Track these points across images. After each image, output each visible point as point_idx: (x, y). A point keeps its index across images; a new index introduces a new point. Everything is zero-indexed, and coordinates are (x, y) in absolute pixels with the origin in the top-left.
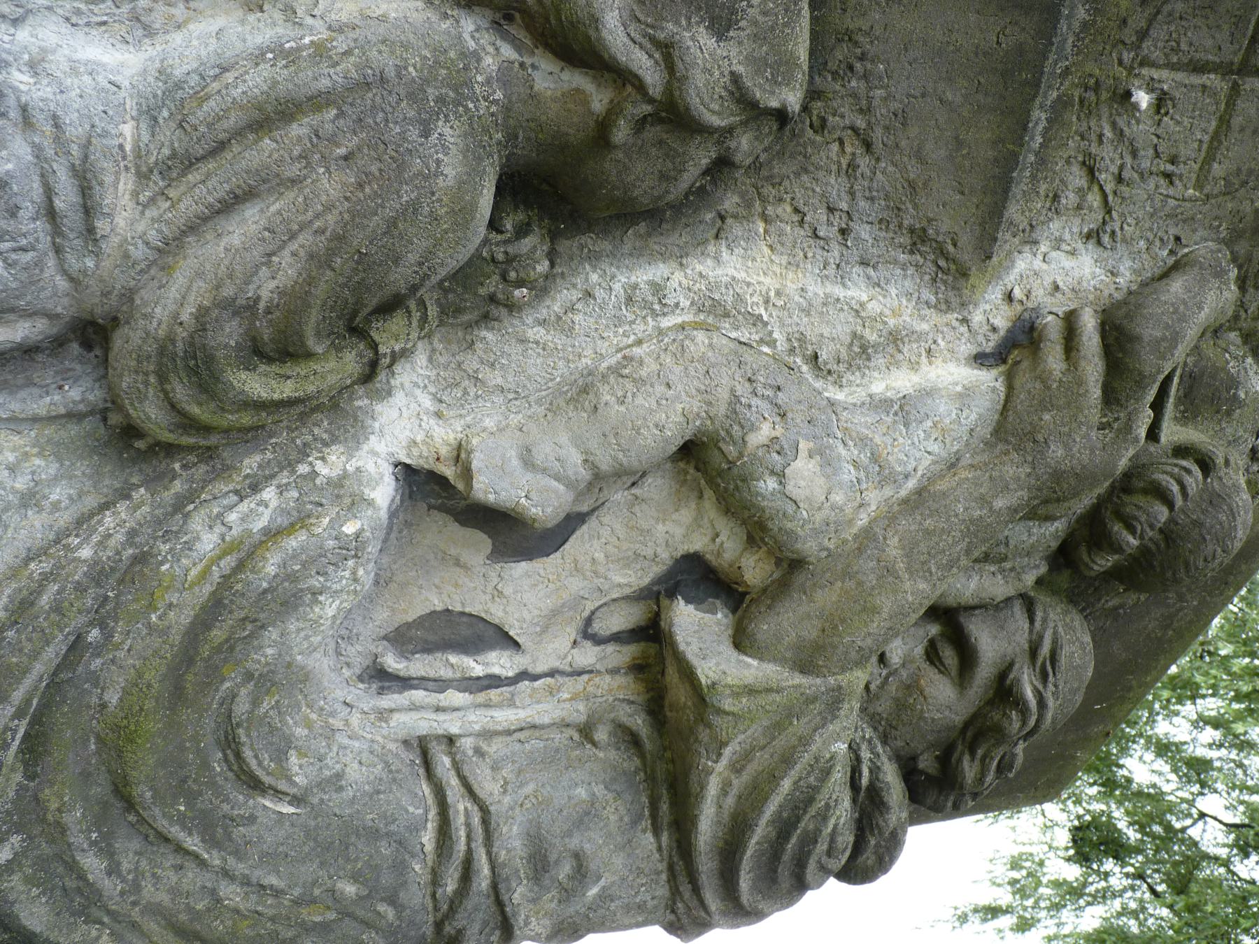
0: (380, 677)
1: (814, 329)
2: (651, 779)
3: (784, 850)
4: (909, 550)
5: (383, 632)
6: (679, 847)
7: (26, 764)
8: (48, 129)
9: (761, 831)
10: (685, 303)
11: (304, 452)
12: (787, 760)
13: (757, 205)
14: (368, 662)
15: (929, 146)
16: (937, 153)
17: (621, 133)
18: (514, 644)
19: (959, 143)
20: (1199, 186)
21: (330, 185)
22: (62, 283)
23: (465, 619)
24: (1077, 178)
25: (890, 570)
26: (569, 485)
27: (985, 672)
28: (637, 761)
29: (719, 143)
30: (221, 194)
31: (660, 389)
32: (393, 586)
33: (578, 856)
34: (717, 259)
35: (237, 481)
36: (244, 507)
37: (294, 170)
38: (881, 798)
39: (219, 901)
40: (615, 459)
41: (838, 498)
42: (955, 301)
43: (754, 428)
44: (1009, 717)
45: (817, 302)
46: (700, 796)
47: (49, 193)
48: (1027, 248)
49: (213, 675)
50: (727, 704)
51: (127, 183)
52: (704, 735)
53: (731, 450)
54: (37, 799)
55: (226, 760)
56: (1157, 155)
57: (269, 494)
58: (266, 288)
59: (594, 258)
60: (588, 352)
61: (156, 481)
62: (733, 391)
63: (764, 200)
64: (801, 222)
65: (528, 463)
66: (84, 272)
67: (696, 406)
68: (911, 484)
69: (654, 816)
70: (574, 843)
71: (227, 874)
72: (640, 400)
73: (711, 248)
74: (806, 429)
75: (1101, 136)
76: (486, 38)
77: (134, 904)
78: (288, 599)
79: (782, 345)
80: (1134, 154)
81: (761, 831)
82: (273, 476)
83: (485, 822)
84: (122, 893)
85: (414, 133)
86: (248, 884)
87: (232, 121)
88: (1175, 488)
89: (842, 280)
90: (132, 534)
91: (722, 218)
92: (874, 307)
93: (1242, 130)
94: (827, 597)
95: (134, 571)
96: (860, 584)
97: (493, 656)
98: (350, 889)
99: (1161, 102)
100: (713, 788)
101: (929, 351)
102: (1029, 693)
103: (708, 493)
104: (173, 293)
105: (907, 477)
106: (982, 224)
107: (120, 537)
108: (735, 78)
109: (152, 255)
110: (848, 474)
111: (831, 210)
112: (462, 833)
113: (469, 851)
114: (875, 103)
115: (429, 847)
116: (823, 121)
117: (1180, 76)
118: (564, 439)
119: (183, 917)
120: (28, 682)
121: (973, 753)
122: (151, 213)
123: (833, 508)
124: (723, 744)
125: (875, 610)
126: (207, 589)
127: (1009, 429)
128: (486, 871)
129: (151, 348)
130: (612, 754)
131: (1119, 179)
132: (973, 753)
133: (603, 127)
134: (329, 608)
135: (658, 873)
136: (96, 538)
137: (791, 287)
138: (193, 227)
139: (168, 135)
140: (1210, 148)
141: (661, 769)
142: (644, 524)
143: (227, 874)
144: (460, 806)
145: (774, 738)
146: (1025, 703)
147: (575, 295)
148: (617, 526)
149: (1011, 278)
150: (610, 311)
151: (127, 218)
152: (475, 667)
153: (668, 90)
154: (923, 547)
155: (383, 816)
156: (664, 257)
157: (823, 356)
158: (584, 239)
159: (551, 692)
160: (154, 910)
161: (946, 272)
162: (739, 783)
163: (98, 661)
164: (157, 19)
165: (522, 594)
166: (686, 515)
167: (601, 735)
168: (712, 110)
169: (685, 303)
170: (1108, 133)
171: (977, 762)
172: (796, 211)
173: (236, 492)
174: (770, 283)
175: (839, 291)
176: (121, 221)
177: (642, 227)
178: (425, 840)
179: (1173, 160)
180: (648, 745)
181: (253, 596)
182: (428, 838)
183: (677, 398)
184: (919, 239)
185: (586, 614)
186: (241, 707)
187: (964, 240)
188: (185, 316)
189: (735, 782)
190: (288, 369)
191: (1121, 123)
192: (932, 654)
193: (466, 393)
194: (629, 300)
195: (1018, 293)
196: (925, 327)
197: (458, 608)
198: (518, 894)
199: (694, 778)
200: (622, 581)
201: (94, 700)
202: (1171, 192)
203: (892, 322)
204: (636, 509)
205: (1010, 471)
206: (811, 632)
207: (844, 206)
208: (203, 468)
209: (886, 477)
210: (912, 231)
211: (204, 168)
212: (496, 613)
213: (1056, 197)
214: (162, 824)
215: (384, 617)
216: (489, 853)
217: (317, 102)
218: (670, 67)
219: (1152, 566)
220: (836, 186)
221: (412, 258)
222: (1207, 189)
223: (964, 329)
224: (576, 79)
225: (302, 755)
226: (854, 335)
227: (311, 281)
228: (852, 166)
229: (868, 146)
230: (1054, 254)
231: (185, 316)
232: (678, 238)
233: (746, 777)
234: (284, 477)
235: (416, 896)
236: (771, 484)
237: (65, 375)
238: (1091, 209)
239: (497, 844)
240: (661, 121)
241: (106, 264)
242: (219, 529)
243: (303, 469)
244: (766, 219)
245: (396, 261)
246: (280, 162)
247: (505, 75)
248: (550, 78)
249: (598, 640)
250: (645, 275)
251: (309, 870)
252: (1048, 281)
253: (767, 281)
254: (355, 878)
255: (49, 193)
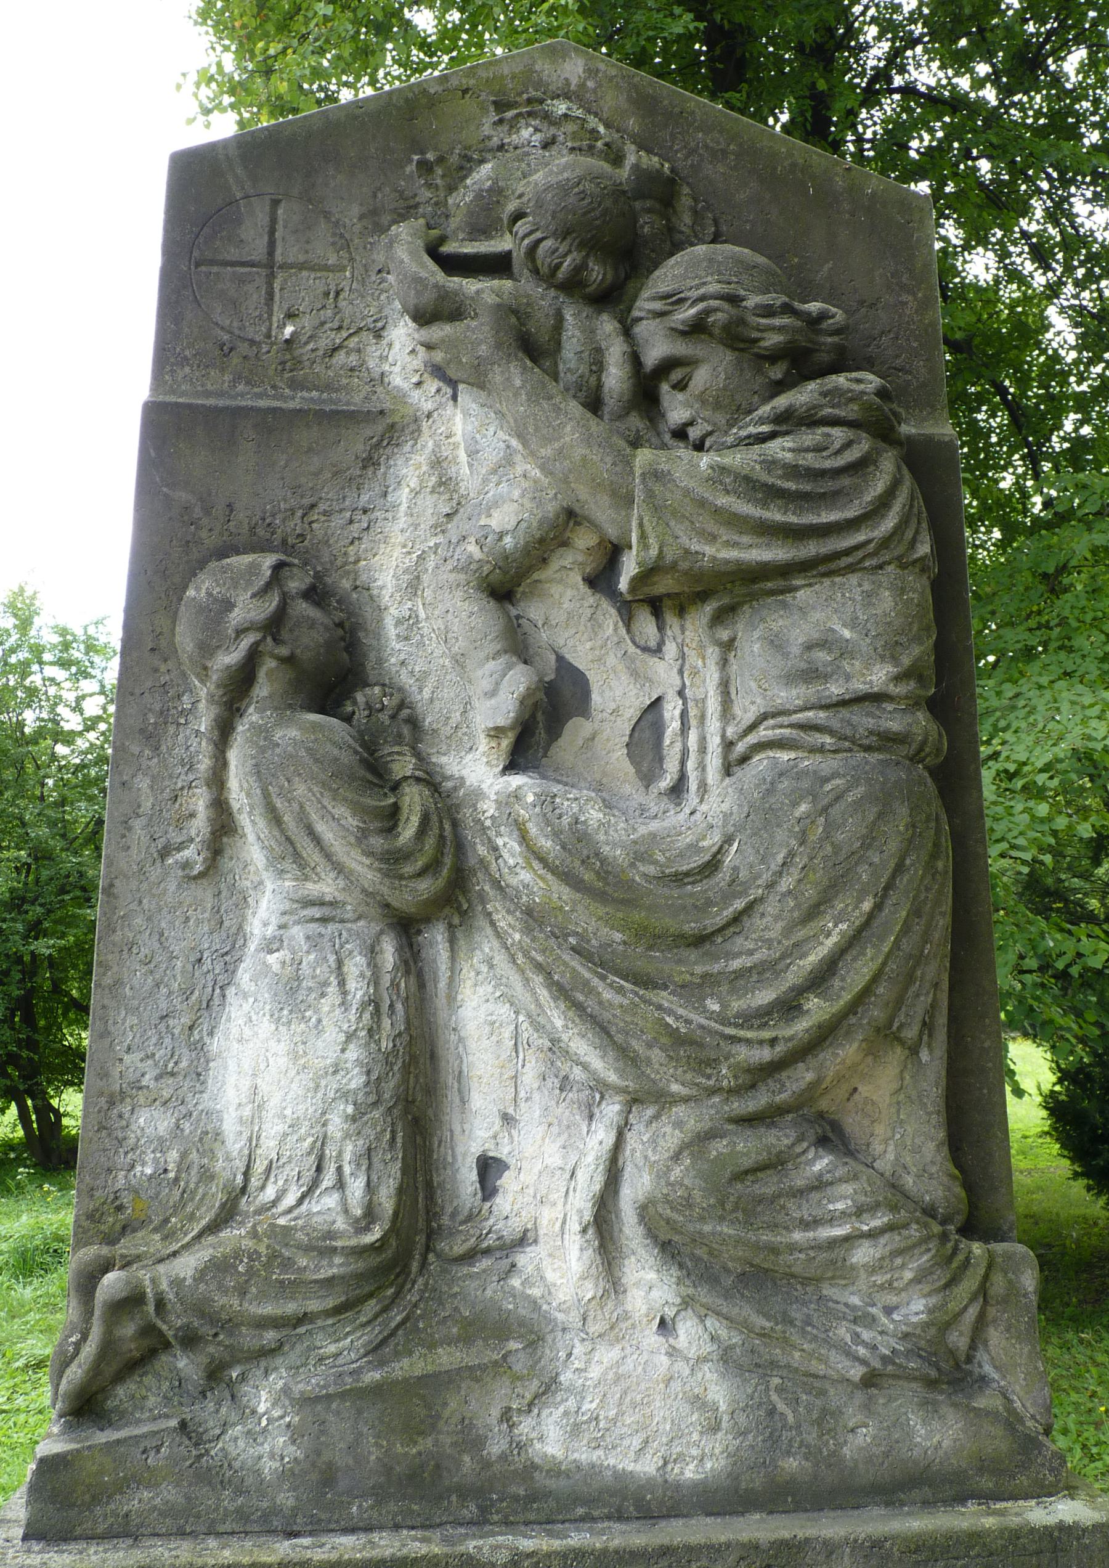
0: (678, 790)
1: (428, 519)
2: (753, 597)
3: (797, 491)
4: (547, 440)
5: (642, 789)
6: (805, 571)
7: (655, 988)
8: (287, 917)
9: (775, 515)
10: (409, 604)
11: (478, 821)
12: (702, 503)
13: (350, 567)
14: (665, 798)
15: (312, 469)
16: (316, 462)
17: (284, 651)
18: (657, 703)
19: (310, 450)
20: (343, 269)
21: (300, 789)
22: (361, 923)
23: (636, 735)
24: (340, 358)
25: (560, 451)
26: (510, 667)
27: (681, 348)
28: (746, 607)
29: (293, 598)
30: (309, 840)
31: (450, 616)
32: (604, 781)
33: (809, 647)
34: (381, 588)
35: (491, 858)
36: (506, 855)
37: (295, 806)
38: (782, 413)
39: (790, 892)
40: (492, 641)
41: (516, 494)
42: (413, 427)
43: (470, 556)
44: (714, 322)
45: (410, 520)
46: (738, 562)
47: (313, 920)
48: (386, 380)
49: (630, 885)
50: (654, 552)
51: (310, 885)
52: (684, 565)
53: (486, 569)
54: (682, 987)
55: (693, 883)
56: (324, 307)
57: (500, 842)
58: (352, 822)
59: (380, 662)
60: (441, 661)
61: (483, 898)
62: (451, 571)
63: (346, 564)
64: (359, 539)
65: (492, 693)
66: (355, 911)
67: (459, 594)
68: (514, 443)
69: (782, 592)
70: (795, 650)
71: (771, 886)
72: (455, 629)
73: (375, 592)
74: (473, 521)
75: (313, 350)
76: (245, 720)
77: (779, 942)
78: (577, 839)
79: (440, 539)
80: (323, 324)
81: (775, 515)
82: (489, 839)
83: (774, 715)
84: (769, 949)
85: (278, 751)
86: (781, 873)
87: (276, 833)
88: (526, 242)
89: (396, 506)
90: (509, 912)
91: (356, 587)
92: (414, 483)
93: (307, 252)
94: (583, 492)
95: (533, 917)
96: (570, 471)
97: (667, 715)
98: (803, 808)
99: (291, 316)
100: (733, 554)
101: (447, 437)
102: (693, 311)
103: (535, 576)
104: (359, 868)
105: (508, 447)
106: (358, 423)
107: (510, 918)
108: (254, 596)
109: (342, 877)
110: (504, 487)
111: (351, 522)
112: (778, 731)
113: (791, 726)
114: (288, 506)
115: (792, 755)
116: (299, 535)
117: (276, 308)
118: (480, 673)
119: (796, 914)
120: (580, 969)
121: (756, 341)
122: (323, 875)
123: (523, 496)
124: (687, 552)
125: (584, 458)
126: (549, 876)
127: (480, 383)
128: (810, 714)
129: (387, 881)
130: (740, 626)
131: (340, 328)
132: (756, 341)
133: (283, 660)
134: (594, 815)
135: (833, 584)
136: (510, 931)
137: (401, 539)
138: (328, 856)
139: (288, 865)
140: (320, 270)
141: (740, 590)
142: (564, 618)
143: (771, 886)
144: (764, 733)
145: (683, 516)
146: (699, 313)
147: (404, 671)
148: (567, 635)
149: (405, 386)
150: (413, 649)
151: (327, 887)
152: (673, 726)
153: (258, 629)
154: (545, 431)
155: (757, 786)
156: (380, 620)
157: (447, 510)
158: (369, 668)
159: (695, 673)
160: (787, 931)
161: (391, 438)
162: (725, 534)
163: (593, 942)
164: (256, 879)
165: (615, 697)
166: (555, 590)
167: (724, 635)
168: (272, 603)
169: (409, 604)
170: (311, 346)
171: (765, 335)
172: (352, 543)
173: (497, 859)
174: (397, 553)
175: (403, 508)
176: (327, 890)
177: (361, 634)
178: (786, 758)
179: (327, 294)
180: (726, 600)
181: (565, 855)
182: (785, 756)
183: (454, 606)
184: (370, 462)
185: (638, 651)
186: (651, 870)
187: (369, 433)
188: (368, 862)
189: (725, 538)
190: (403, 818)
191: (304, 339)
192: (681, 386)
193: (465, 734)
194: (407, 639)
195: (415, 380)
196: (430, 444)
197: (627, 739)
198: (835, 690)
199: (723, 568)
200: (611, 627)
201: (621, 948)
202: (347, 288)
203: (424, 468)
204: (554, 623)
205: (498, 378)
206: (605, 500)
207: (348, 514)
208: (479, 874)
209: (508, 461)
210: (364, 467)
211: (299, 849)
212: (632, 709)
213: (352, 370)
214: (719, 921)
215: (629, 788)
216: (795, 712)
217: (266, 795)
218: (246, 630)
219: (593, 236)
220: (338, 521)
221: (336, 752)
222: (345, 262)
223: (435, 414)
224: (262, 675)
225: (704, 838)
226: (432, 492)
227: (345, 799)
228: (325, 513)
229: (313, 506)
230: (390, 359)
231: (368, 862)
232: (368, 613)
233: (722, 531)
234: (492, 833)
235: (828, 764)
236: (508, 540)
237: (432, 944)
238: (359, 343)
239: (787, 706)
240: (279, 631)
241: (349, 900)
242: (518, 870)
243: (488, 823)
244: (358, 561)
245: (337, 759)
246: (292, 812)
247: (260, 710)
248: (262, 689)
249: (661, 645)
250: (391, 630)
251: (780, 835)
252: (408, 359)
253: (395, 555)
254: (795, 804)
255: (313, 920)
